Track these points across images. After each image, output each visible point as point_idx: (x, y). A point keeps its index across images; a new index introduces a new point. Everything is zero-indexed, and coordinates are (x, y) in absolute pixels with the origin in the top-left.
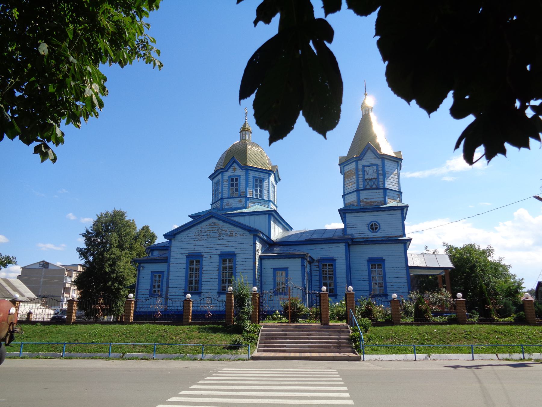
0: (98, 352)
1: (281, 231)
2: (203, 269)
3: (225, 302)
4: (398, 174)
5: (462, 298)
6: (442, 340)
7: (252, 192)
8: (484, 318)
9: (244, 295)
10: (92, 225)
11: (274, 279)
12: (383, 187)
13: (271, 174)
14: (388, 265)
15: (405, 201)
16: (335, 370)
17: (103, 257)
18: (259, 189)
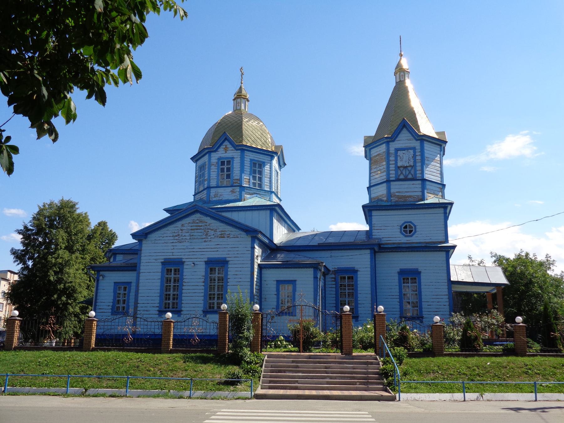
0: (51, 386)
1: (286, 231)
2: (184, 280)
3: (216, 324)
4: (441, 161)
5: (522, 323)
6: (497, 376)
7: (249, 179)
8: (549, 349)
9: (243, 315)
10: (31, 219)
11: (278, 294)
12: (421, 178)
13: (274, 157)
14: (424, 278)
15: (449, 197)
16: (367, 413)
17: (47, 262)
18: (257, 176)
